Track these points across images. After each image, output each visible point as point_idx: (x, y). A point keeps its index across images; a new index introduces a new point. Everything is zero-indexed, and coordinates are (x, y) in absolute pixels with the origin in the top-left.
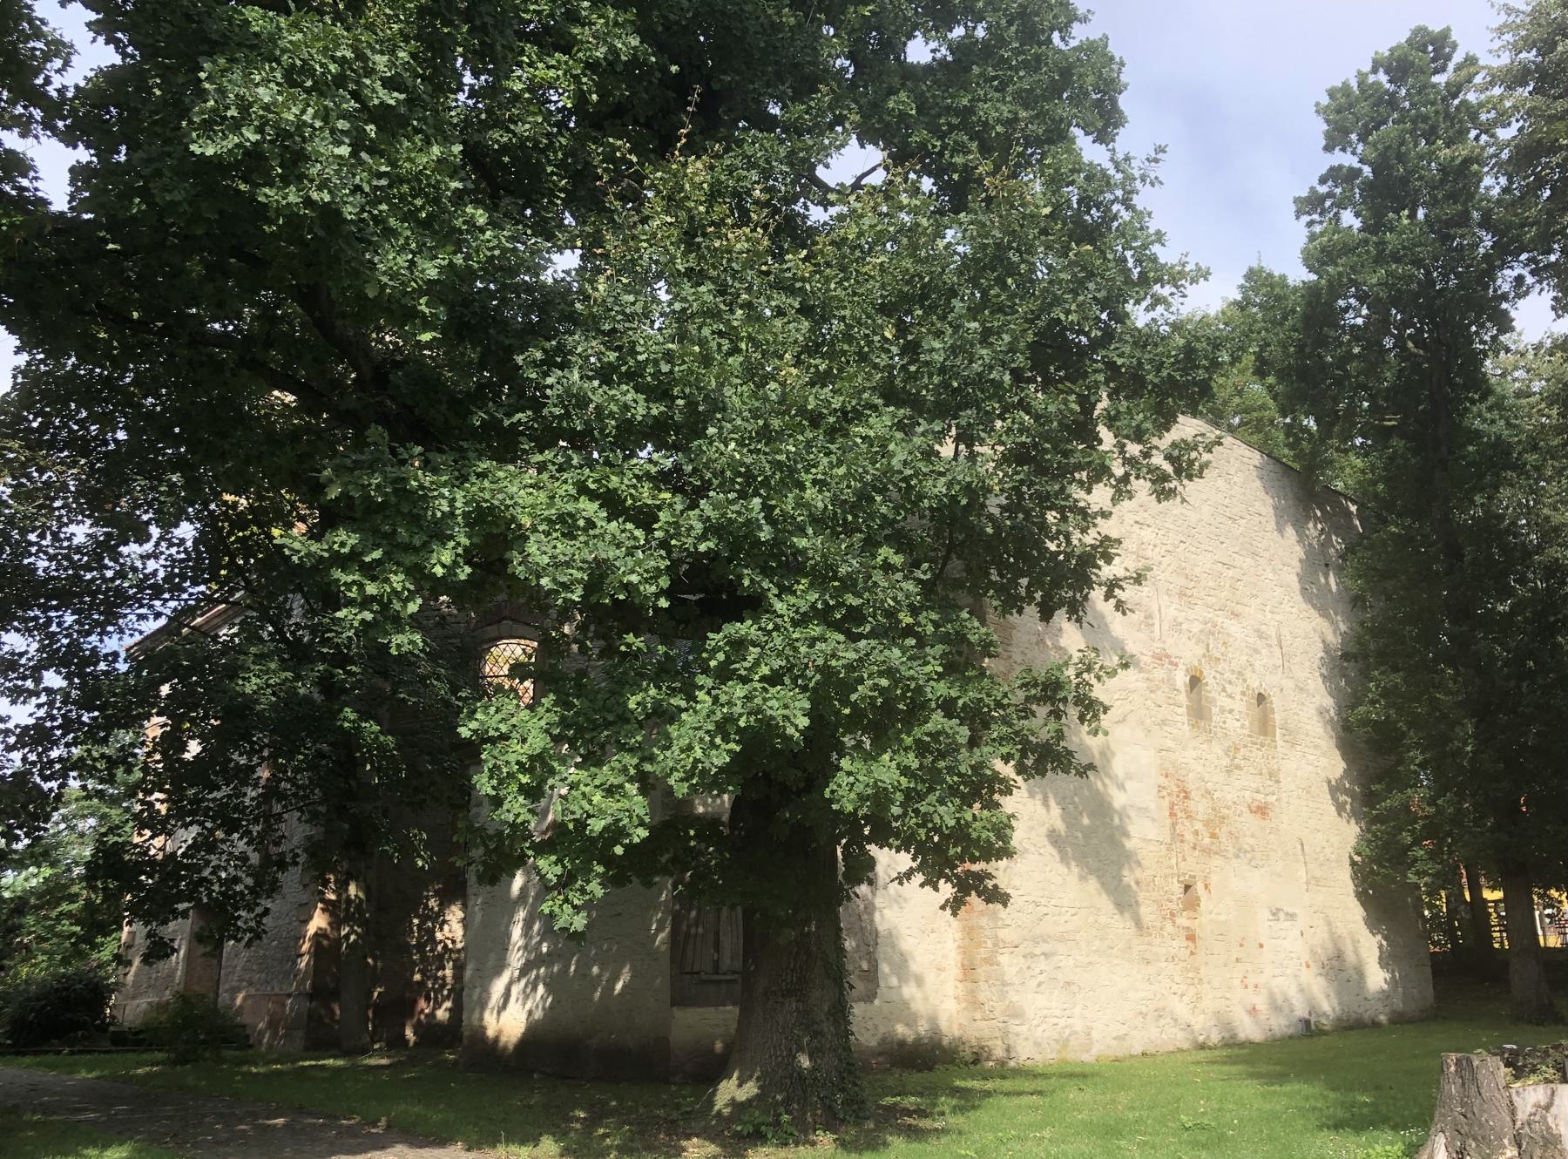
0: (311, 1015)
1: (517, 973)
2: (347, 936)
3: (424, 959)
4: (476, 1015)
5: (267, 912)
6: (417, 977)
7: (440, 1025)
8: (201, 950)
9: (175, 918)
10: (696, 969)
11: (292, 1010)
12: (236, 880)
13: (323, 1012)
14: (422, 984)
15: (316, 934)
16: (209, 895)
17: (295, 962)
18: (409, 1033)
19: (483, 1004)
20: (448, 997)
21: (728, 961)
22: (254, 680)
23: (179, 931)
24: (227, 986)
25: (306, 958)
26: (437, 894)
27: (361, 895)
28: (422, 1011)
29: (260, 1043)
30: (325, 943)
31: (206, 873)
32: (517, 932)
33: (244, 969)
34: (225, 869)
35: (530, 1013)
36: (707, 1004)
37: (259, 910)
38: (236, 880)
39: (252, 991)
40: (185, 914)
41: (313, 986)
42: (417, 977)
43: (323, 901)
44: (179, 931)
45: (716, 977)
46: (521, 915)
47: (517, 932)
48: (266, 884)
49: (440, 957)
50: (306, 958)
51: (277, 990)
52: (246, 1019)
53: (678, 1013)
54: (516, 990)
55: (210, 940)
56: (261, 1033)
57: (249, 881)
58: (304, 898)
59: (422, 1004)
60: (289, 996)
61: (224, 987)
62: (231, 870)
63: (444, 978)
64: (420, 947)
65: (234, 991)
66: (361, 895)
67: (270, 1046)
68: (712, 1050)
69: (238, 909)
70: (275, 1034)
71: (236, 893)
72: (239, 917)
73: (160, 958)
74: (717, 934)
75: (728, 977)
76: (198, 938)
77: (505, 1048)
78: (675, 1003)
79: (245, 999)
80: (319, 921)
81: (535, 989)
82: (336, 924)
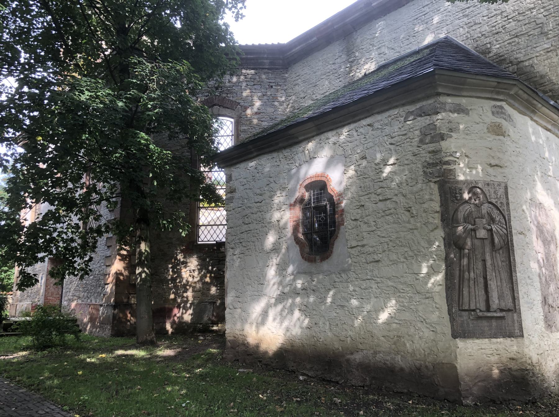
0: (114, 316)
1: (273, 301)
2: (140, 274)
3: (176, 287)
4: (238, 326)
5: (91, 259)
6: (172, 296)
7: (186, 323)
8: (53, 280)
9: (37, 262)
10: (473, 307)
11: (103, 313)
12: (72, 240)
13: (121, 315)
14: (175, 300)
15: (116, 273)
16: (57, 249)
17: (103, 287)
18: (168, 327)
19: (244, 320)
20: (190, 308)
21: (497, 301)
22: (87, 93)
23: (41, 269)
24: (66, 298)
25: (110, 286)
26: (182, 251)
27: (147, 249)
28: (175, 315)
29: (85, 329)
30: (121, 278)
31: (55, 235)
32: (271, 272)
33: (75, 290)
34: (66, 233)
35: (288, 329)
36: (481, 335)
37: (87, 259)
38: (72, 240)
39: (80, 302)
40: (42, 260)
41: (115, 301)
42: (172, 296)
43: (120, 255)
44: (41, 269)
45: (489, 314)
46: (275, 260)
47: (271, 272)
48: (88, 246)
49: (185, 286)
50: (110, 286)
51: (93, 302)
52: (78, 316)
53: (460, 343)
54: (272, 313)
55: (57, 275)
56: (86, 325)
57: (80, 241)
58: (108, 253)
59: (176, 311)
60: (101, 305)
61: (65, 299)
62: (70, 234)
63: (187, 297)
64: (173, 280)
65: (71, 301)
66: (147, 249)
67: (91, 332)
68: (491, 376)
69: (74, 257)
70: (93, 326)
71: (73, 248)
72: (75, 262)
73: (28, 286)
74: (485, 278)
75: (499, 314)
76: (52, 274)
77: (266, 353)
78: (455, 336)
79: (76, 305)
80: (118, 266)
81: (291, 312)
82: (131, 267)
